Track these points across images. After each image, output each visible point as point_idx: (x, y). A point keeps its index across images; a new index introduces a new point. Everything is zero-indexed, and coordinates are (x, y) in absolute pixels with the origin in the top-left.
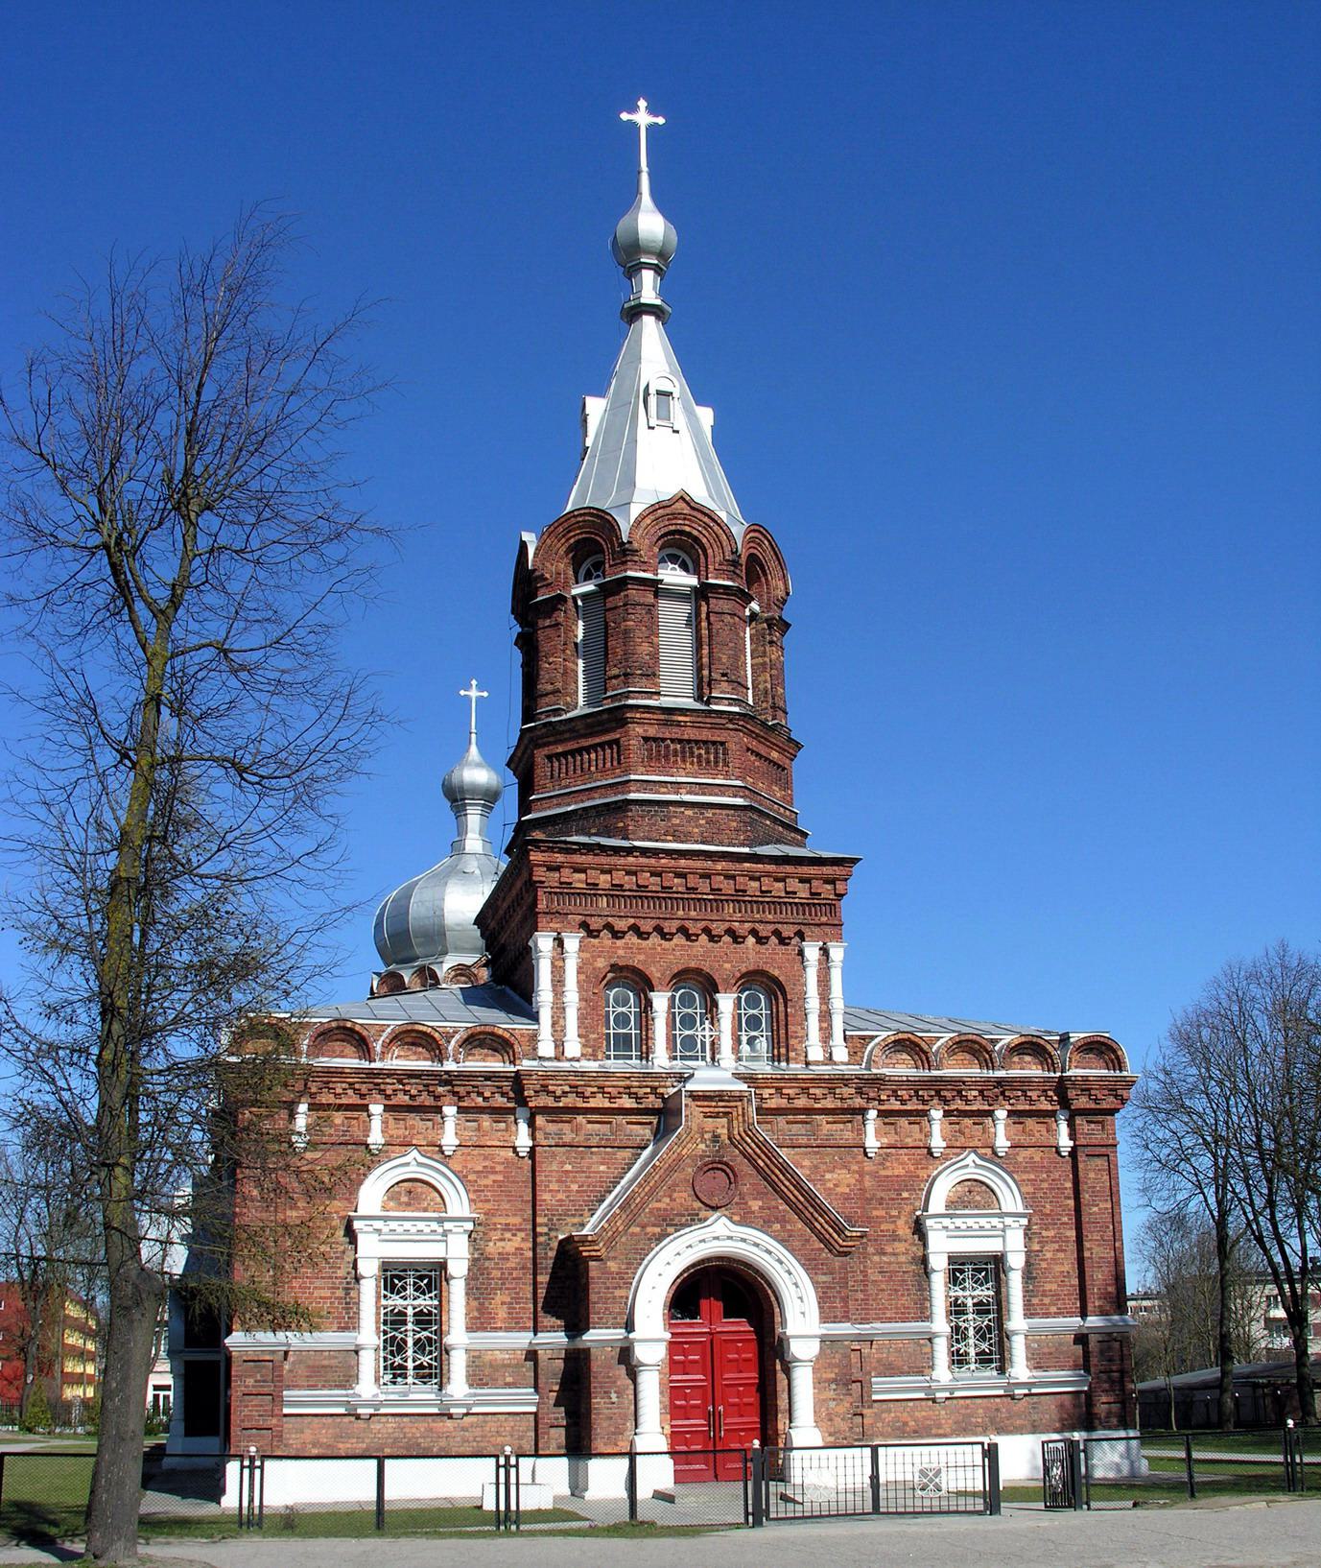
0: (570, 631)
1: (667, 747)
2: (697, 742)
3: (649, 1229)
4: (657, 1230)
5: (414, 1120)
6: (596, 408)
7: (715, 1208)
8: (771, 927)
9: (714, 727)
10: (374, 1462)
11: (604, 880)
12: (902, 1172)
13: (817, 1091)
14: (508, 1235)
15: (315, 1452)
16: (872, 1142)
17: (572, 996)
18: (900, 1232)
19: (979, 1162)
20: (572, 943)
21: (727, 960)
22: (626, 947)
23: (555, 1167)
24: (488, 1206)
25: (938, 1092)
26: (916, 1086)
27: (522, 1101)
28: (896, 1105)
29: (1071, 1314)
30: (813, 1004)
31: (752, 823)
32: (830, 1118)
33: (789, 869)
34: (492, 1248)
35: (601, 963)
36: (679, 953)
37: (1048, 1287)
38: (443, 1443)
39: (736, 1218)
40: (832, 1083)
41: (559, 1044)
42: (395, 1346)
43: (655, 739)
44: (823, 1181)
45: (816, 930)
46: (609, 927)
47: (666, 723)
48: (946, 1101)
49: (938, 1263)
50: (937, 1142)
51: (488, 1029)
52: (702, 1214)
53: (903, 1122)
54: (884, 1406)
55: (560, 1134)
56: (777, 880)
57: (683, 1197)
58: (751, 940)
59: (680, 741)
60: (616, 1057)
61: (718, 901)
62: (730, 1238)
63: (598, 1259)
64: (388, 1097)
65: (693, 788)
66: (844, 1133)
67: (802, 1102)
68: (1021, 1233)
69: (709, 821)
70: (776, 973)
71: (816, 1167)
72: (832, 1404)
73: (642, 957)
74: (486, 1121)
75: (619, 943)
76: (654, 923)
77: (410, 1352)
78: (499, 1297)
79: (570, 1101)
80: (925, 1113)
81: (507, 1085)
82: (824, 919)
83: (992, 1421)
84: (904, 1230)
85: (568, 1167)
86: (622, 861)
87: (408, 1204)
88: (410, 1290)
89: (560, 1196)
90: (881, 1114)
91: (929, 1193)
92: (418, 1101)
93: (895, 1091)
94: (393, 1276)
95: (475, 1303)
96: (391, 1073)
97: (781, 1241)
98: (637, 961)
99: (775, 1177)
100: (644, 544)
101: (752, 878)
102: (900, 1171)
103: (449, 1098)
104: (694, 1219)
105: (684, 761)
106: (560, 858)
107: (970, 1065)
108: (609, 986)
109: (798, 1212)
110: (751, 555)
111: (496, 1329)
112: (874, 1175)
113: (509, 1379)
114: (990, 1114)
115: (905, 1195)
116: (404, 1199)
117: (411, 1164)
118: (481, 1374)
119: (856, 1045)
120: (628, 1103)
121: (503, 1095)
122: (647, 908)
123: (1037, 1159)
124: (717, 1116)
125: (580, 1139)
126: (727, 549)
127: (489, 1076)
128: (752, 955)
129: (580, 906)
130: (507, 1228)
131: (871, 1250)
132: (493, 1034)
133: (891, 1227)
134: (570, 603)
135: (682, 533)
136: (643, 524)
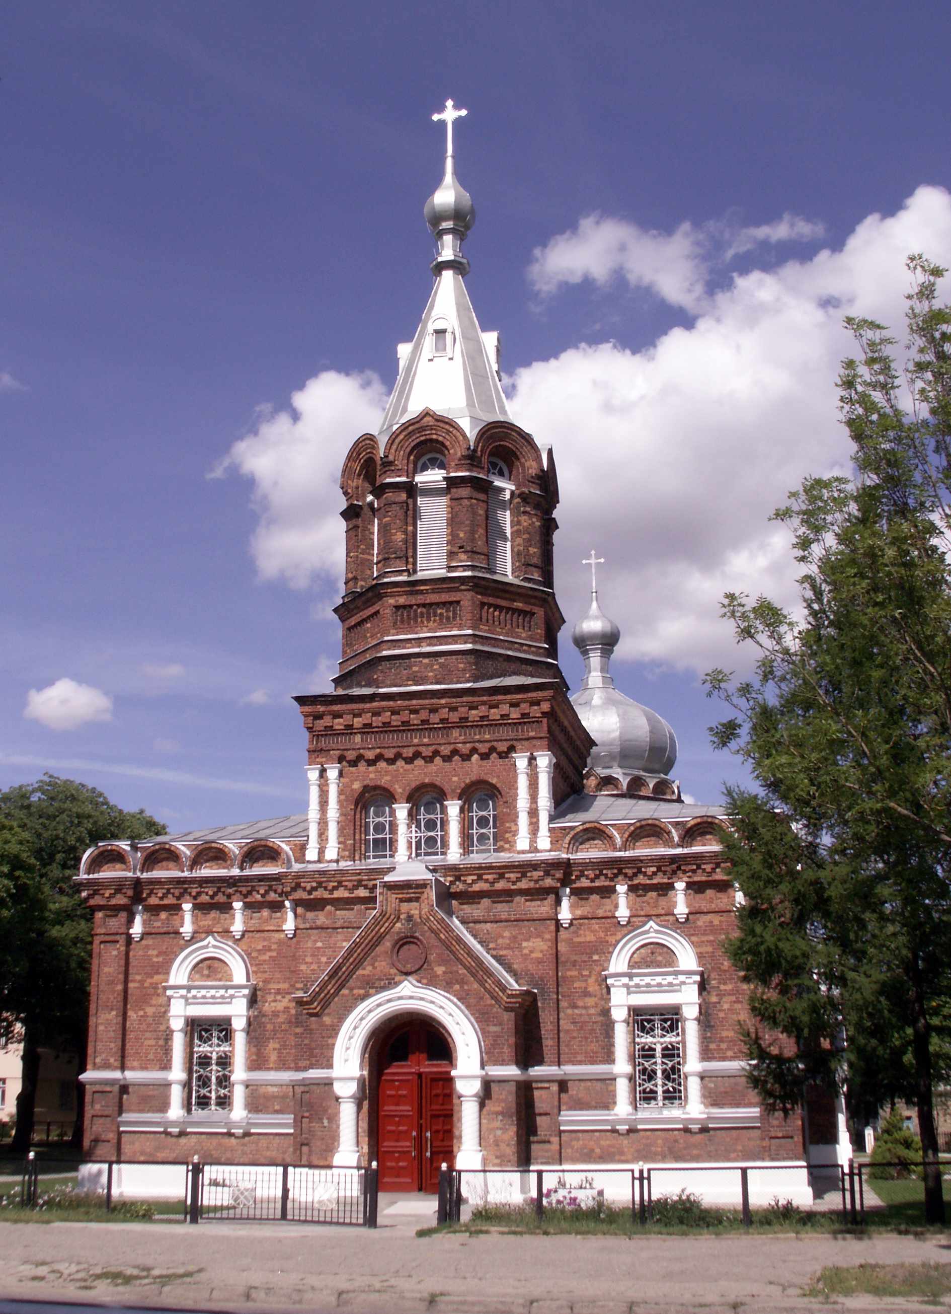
1: (416, 611)
2: (437, 604)
3: (356, 991)
4: (362, 992)
7: (407, 974)
8: (488, 745)
9: (450, 590)
10: (280, 1169)
13: (512, 875)
14: (279, 997)
15: (142, 1159)
16: (565, 914)
18: (590, 989)
20: (332, 774)
22: (376, 771)
29: (115, 1069)
34: (267, 1007)
35: (357, 786)
37: (725, 1034)
38: (229, 1155)
39: (425, 981)
41: (321, 851)
42: (224, 1081)
43: (404, 607)
44: (520, 948)
45: (526, 743)
47: (411, 593)
49: (619, 1014)
51: (263, 843)
52: (397, 979)
54: (573, 1135)
59: (424, 605)
60: (374, 857)
64: (195, 898)
65: (431, 640)
66: (542, 908)
67: (500, 885)
68: (696, 987)
69: (442, 666)
71: (515, 937)
72: (499, 1133)
73: (388, 778)
75: (371, 769)
76: (394, 751)
77: (214, 1087)
78: (272, 1045)
79: (320, 893)
82: (532, 734)
83: (671, 1150)
85: (319, 944)
86: (368, 705)
88: (658, 1031)
89: (314, 967)
94: (642, 1019)
96: (192, 881)
98: (384, 781)
102: (590, 937)
106: (321, 709)
109: (473, 975)
111: (269, 1069)
113: (277, 1107)
115: (596, 957)
116: (206, 972)
117: (211, 946)
118: (255, 1104)
121: (275, 891)
123: (716, 922)
124: (410, 900)
128: (475, 769)
132: (266, 846)
133: (583, 985)
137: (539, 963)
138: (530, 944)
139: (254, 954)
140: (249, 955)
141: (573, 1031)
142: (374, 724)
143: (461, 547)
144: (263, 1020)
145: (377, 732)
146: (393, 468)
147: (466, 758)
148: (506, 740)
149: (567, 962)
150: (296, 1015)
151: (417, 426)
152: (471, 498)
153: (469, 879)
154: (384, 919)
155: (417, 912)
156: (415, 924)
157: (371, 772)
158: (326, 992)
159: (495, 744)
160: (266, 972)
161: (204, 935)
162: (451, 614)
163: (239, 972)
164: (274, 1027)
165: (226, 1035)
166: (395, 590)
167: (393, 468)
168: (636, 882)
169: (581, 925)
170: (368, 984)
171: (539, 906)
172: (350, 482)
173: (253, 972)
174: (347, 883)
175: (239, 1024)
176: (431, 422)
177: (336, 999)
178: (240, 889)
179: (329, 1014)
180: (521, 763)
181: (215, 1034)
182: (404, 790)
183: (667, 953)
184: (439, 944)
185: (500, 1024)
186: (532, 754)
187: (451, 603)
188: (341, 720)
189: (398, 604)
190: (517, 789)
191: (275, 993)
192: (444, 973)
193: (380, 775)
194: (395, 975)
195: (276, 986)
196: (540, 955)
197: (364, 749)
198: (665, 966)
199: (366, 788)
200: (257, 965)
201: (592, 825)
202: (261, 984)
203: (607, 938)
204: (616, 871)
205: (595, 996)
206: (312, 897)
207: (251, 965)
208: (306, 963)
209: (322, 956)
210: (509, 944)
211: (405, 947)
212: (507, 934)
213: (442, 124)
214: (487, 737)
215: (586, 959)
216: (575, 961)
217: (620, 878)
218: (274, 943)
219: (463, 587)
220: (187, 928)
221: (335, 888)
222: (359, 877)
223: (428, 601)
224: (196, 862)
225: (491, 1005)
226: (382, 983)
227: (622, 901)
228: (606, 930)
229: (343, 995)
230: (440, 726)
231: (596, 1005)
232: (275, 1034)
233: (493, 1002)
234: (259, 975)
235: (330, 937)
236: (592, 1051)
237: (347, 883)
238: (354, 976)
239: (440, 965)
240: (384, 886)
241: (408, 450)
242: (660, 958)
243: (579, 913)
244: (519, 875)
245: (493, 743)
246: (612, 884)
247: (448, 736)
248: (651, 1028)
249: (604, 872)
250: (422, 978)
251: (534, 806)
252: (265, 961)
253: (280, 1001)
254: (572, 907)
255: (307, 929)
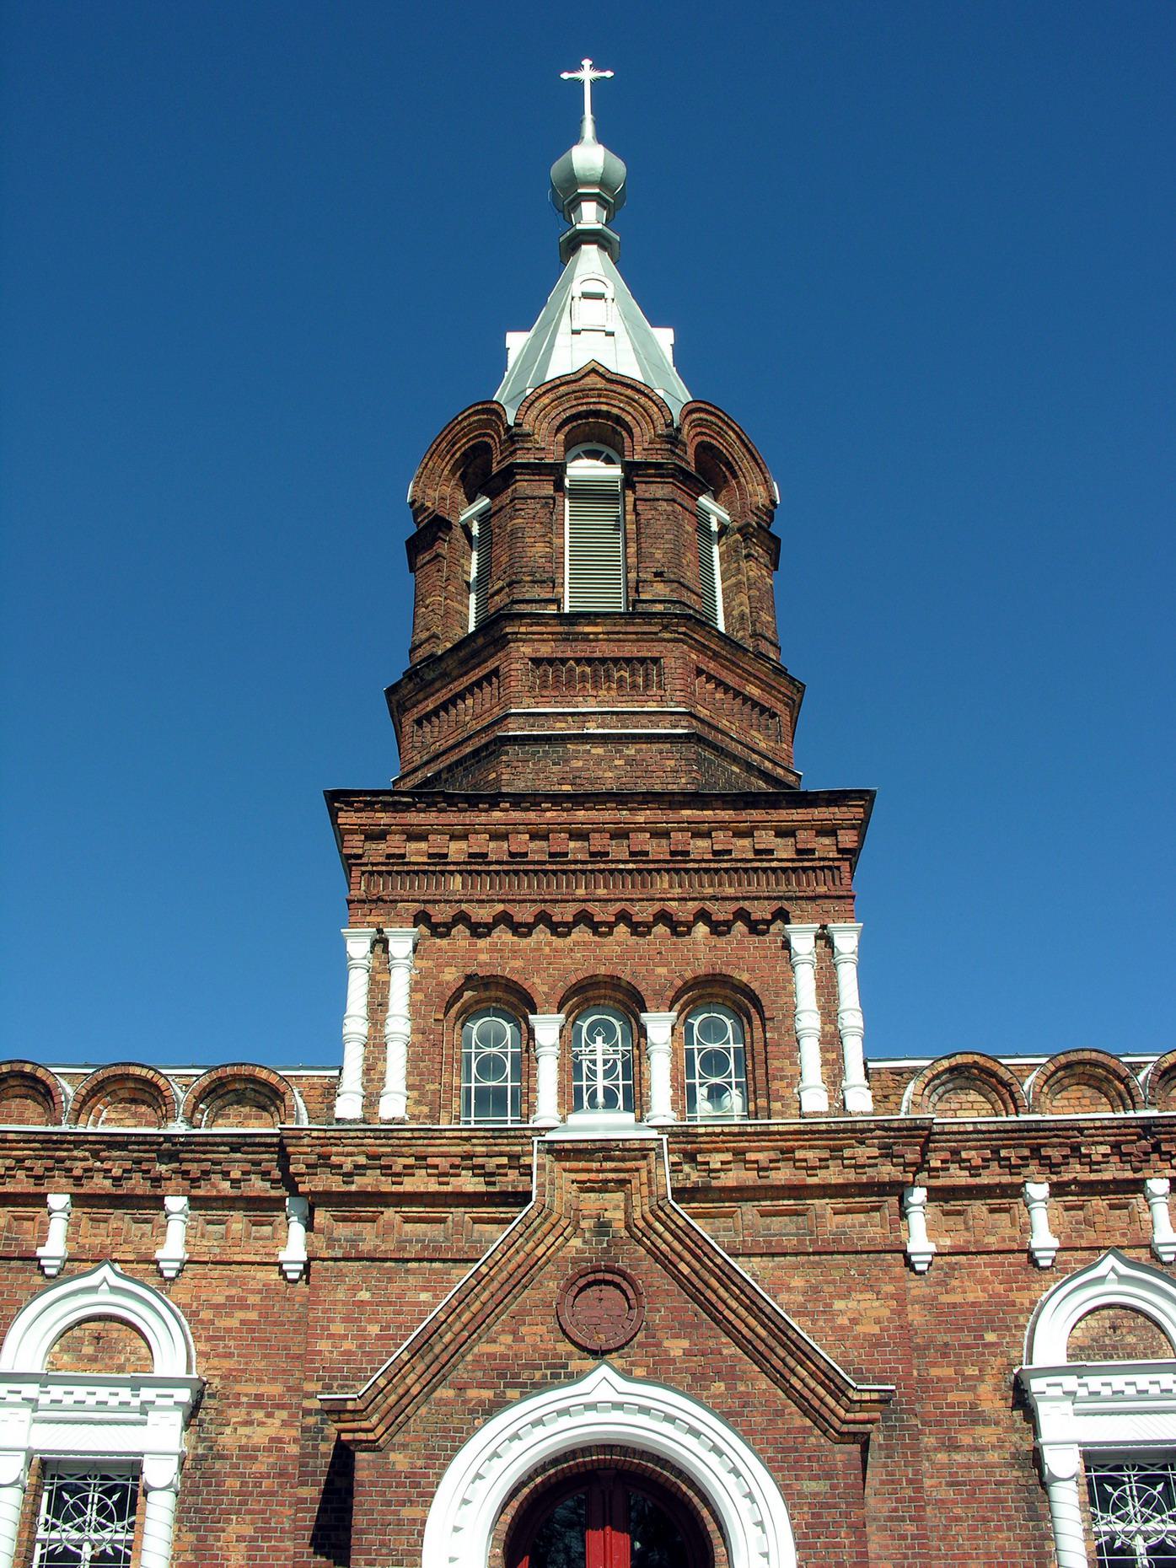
0: (458, 564)
1: (571, 670)
2: (616, 661)
3: (472, 1393)
4: (487, 1394)
5: (119, 1219)
6: (516, 342)
7: (598, 1354)
8: (733, 906)
9: (642, 637)
11: (457, 850)
12: (982, 1297)
13: (810, 1154)
14: (259, 1415)
16: (920, 1240)
17: (399, 1024)
18: (985, 1407)
19: (1124, 1270)
20: (401, 945)
21: (660, 961)
22: (493, 949)
23: (341, 1295)
24: (228, 1364)
25: (1035, 1150)
26: (996, 1141)
27: (289, 1182)
28: (960, 1177)
30: (809, 1020)
31: (699, 761)
32: (839, 1203)
33: (756, 815)
34: (228, 1439)
35: (451, 976)
36: (581, 955)
39: (639, 1372)
40: (838, 1135)
43: (550, 661)
45: (809, 907)
46: (462, 918)
47: (567, 638)
48: (1051, 1166)
49: (1063, 1462)
50: (1043, 1239)
52: (574, 1365)
53: (978, 1208)
55: (353, 1242)
56: (739, 834)
57: (538, 1334)
58: (701, 929)
59: (589, 661)
61: (643, 868)
62: (618, 1406)
63: (371, 1446)
66: (869, 1228)
67: (783, 1175)
69: (630, 761)
70: (745, 977)
71: (816, 1290)
73: (518, 964)
74: (238, 1222)
75: (482, 943)
76: (535, 908)
78: (237, 1527)
79: (369, 1181)
80: (1017, 1191)
81: (269, 1160)
82: (822, 889)
84: (992, 1401)
85: (364, 1295)
87: (93, 1359)
88: (91, 1514)
89: (348, 1345)
90: (935, 1194)
91: (1033, 1331)
92: (126, 1188)
93: (955, 1152)
95: (191, 1537)
96: (79, 1141)
97: (726, 1416)
98: (511, 968)
99: (710, 1293)
100: (546, 442)
101: (697, 835)
102: (976, 1294)
103: (177, 1181)
104: (560, 1374)
105: (595, 687)
106: (384, 818)
107: (1095, 1104)
108: (469, 1013)
109: (759, 1358)
110: (701, 445)
112: (930, 1303)
114: (1138, 1186)
115: (990, 1337)
116: (88, 1350)
117: (102, 1291)
119: (886, 1086)
120: (469, 1183)
121: (265, 1175)
122: (525, 887)
124: (603, 1187)
125: (388, 1247)
126: (660, 422)
127: (238, 1144)
128: (703, 953)
129: (423, 888)
130: (258, 1402)
131: (929, 1441)
133: (968, 1397)
134: (458, 533)
135: (597, 414)
136: (538, 405)
137: (876, 1345)
138: (852, 1304)
139: (205, 1315)
140: (192, 1316)
141: (954, 1502)
142: (492, 857)
143: (656, 574)
144: (218, 1465)
145: (497, 872)
146: (529, 445)
147: (679, 928)
148: (768, 898)
149: (927, 1348)
150: (303, 1455)
151: (574, 387)
152: (674, 501)
153: (716, 1160)
154: (546, 1226)
155: (620, 1215)
156: (615, 1242)
157: (481, 951)
158: (401, 1391)
159: (746, 904)
160: (231, 1355)
161: (90, 1266)
162: (640, 681)
163: (171, 1352)
164: (244, 1484)
165: (120, 1504)
166: (535, 629)
167: (529, 445)
168: (1067, 1177)
169: (952, 1267)
170: (502, 1376)
171: (863, 1225)
172: (429, 491)
173: (200, 1354)
174: (436, 1161)
175: (160, 1473)
176: (601, 384)
177: (423, 1410)
178: (185, 1166)
179: (404, 1446)
180: (803, 941)
181: (94, 1496)
182: (552, 988)
183: (1145, 1327)
184: (676, 1287)
185: (828, 1477)
186: (824, 927)
187: (642, 661)
188: (423, 845)
189: (538, 655)
190: (793, 994)
191: (251, 1406)
192: (687, 1353)
193: (499, 954)
194: (569, 1356)
195: (252, 1389)
196: (876, 1330)
197: (468, 901)
198: (1145, 1356)
199: (470, 981)
200: (209, 1339)
201: (969, 1059)
202: (216, 1382)
203: (1013, 1296)
204: (1026, 1152)
205: (997, 1423)
206: (353, 1188)
207: (197, 1339)
208: (330, 1336)
209: (369, 1321)
210: (803, 1305)
211: (592, 1292)
212: (797, 1282)
213: (580, 67)
214: (730, 891)
215: (970, 1341)
216: (946, 1345)
217: (1033, 1167)
218: (253, 1292)
219: (667, 636)
220: (54, 1247)
221: (408, 1170)
222: (467, 1148)
223: (598, 655)
224: (85, 1103)
225: (804, 1429)
226: (538, 1374)
227: (1040, 1217)
228: (1009, 1281)
229: (442, 1402)
230: (631, 866)
231: (1000, 1445)
232: (243, 1503)
233: (809, 1423)
234: (215, 1362)
235: (390, 1280)
236: (1001, 1548)
237: (436, 1161)
238: (469, 1358)
239: (677, 1336)
240: (549, 1152)
241: (557, 423)
242: (1131, 1339)
243: (947, 1242)
244: (825, 1154)
245: (742, 904)
246: (1018, 1179)
247: (643, 886)
248: (1120, 1498)
249: (1003, 1153)
250: (633, 1364)
251: (829, 1028)
252: (229, 1330)
253: (261, 1424)
254: (932, 1230)
255: (336, 1259)
